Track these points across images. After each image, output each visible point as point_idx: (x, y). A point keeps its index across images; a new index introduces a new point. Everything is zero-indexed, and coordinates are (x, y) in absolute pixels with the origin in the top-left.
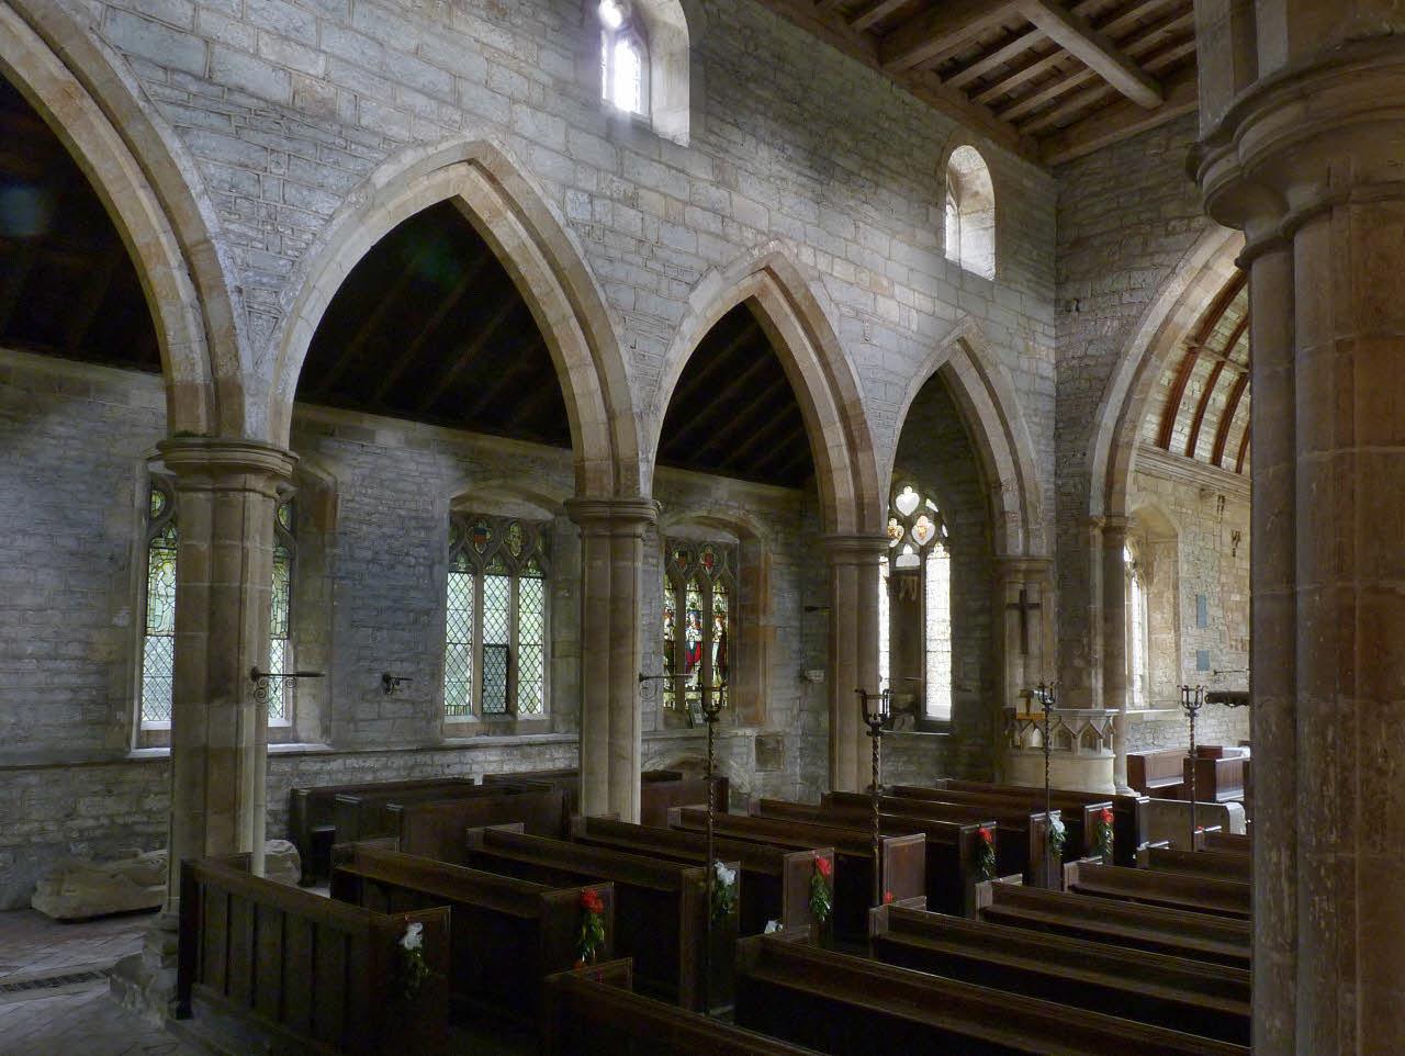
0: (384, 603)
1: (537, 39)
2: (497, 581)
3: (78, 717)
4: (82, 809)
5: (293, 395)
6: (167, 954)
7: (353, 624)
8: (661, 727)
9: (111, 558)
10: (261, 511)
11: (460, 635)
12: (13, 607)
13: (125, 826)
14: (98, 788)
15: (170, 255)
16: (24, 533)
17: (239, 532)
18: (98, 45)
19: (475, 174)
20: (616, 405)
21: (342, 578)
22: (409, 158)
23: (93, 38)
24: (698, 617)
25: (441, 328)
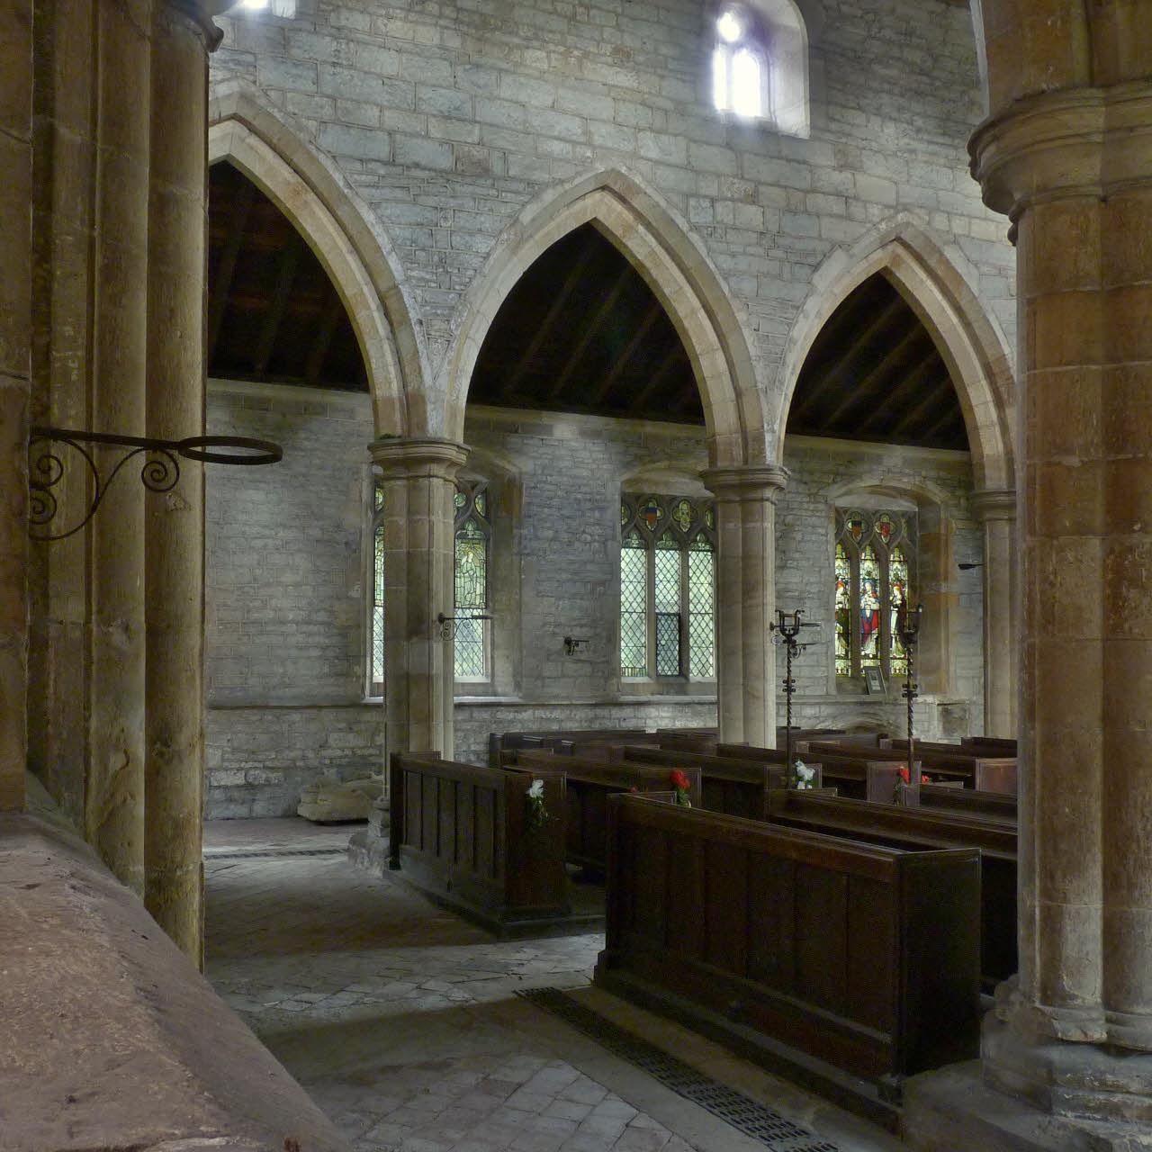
0: (564, 576)
1: (659, 71)
2: (668, 555)
3: (326, 670)
4: (331, 741)
5: (465, 399)
6: (384, 826)
7: (539, 594)
8: (833, 691)
9: (346, 543)
10: (443, 497)
11: (635, 605)
12: (279, 583)
13: (363, 757)
14: (342, 725)
15: (370, 300)
16: (284, 526)
17: (427, 510)
18: (314, 151)
19: (608, 198)
20: (742, 384)
21: (528, 554)
22: (549, 196)
23: (312, 148)
24: (874, 586)
25: (585, 333)
